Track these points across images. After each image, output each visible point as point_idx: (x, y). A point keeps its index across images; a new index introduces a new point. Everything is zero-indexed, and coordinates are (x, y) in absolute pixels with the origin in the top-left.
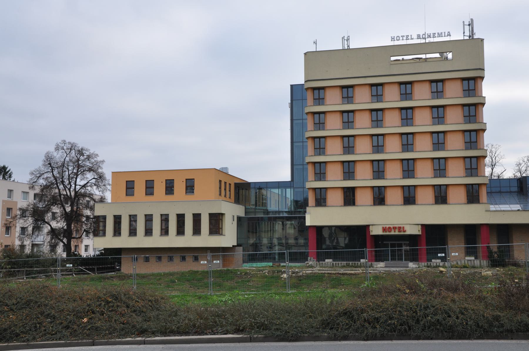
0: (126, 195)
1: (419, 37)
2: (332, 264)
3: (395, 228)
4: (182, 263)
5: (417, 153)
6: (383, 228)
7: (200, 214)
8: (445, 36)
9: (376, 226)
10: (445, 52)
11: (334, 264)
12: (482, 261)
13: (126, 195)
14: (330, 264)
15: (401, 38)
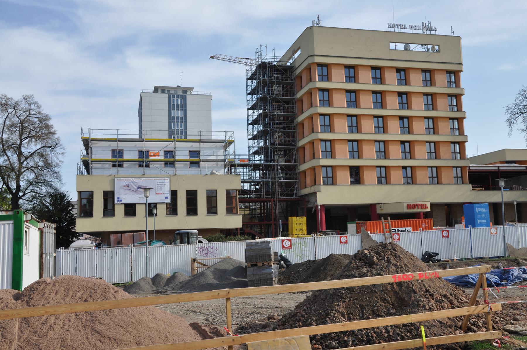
10: (426, 45)
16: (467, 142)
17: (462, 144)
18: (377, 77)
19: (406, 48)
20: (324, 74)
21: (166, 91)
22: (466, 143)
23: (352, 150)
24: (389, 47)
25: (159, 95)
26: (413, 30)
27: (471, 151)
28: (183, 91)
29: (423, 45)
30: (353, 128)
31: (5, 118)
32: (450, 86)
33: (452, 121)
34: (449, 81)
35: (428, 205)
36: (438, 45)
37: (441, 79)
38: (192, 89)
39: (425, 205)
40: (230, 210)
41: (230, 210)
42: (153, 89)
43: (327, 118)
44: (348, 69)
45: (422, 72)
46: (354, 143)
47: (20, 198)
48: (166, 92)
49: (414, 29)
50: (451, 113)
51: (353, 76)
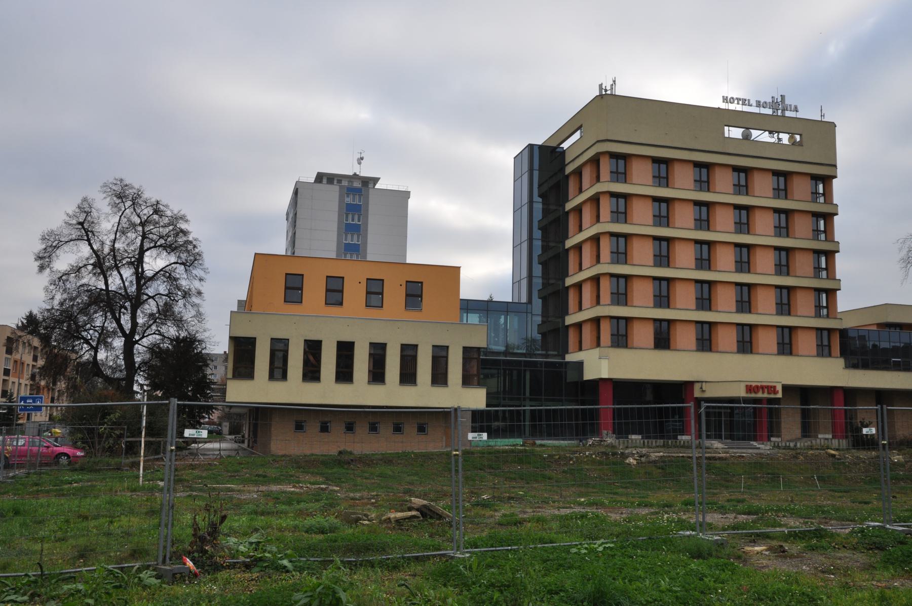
0: (285, 301)
1: (758, 104)
2: (642, 442)
3: (763, 388)
4: (397, 435)
5: (757, 276)
6: (747, 386)
7: (415, 347)
8: (791, 111)
9: (712, 384)
10: (776, 132)
11: (646, 443)
12: (841, 441)
13: (285, 301)
14: (640, 442)
15: (736, 102)
16: (840, 290)
17: (831, 293)
18: (661, 175)
19: (747, 137)
20: (661, 175)
21: (335, 182)
22: (838, 292)
23: (616, 292)
24: (723, 133)
25: (324, 186)
26: (762, 108)
27: (844, 303)
28: (362, 182)
29: (771, 132)
30: (662, 258)
31: (120, 214)
32: (815, 200)
33: (699, 245)
34: (814, 191)
35: (779, 388)
36: (801, 135)
37: (801, 188)
38: (376, 180)
39: (775, 387)
40: (467, 381)
41: (467, 381)
42: (315, 177)
43: (705, 247)
44: (657, 165)
45: (773, 175)
46: (743, 287)
47: (137, 342)
48: (335, 183)
49: (763, 107)
50: (816, 242)
51: (665, 176)
